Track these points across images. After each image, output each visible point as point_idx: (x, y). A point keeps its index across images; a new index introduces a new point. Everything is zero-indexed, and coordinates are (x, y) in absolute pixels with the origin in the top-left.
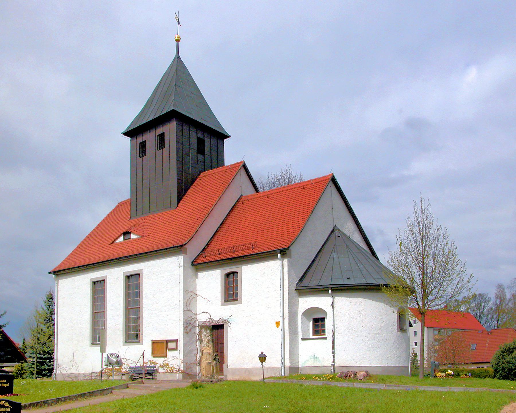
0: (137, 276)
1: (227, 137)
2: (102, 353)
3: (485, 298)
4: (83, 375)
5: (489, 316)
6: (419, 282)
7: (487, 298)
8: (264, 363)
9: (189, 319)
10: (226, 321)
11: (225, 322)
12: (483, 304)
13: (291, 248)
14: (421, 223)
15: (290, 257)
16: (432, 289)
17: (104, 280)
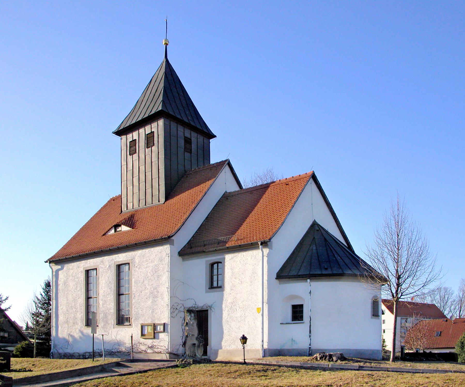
0: (203, 355)
1: (214, 136)
2: (93, 334)
3: (449, 291)
4: (78, 355)
5: (452, 308)
6: (394, 272)
7: (451, 291)
8: (245, 344)
9: (175, 305)
10: (210, 307)
11: (209, 307)
12: (446, 296)
13: (272, 240)
14: (397, 216)
15: (271, 248)
16: (406, 278)
17: (96, 269)
